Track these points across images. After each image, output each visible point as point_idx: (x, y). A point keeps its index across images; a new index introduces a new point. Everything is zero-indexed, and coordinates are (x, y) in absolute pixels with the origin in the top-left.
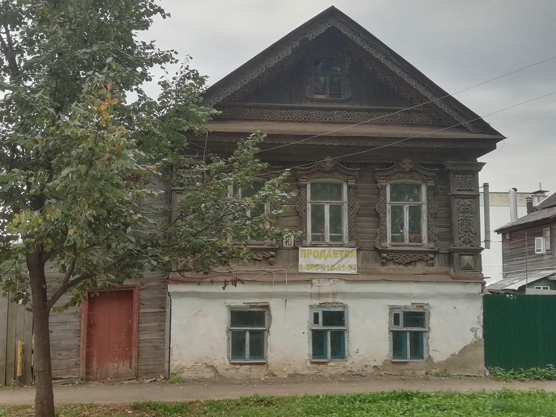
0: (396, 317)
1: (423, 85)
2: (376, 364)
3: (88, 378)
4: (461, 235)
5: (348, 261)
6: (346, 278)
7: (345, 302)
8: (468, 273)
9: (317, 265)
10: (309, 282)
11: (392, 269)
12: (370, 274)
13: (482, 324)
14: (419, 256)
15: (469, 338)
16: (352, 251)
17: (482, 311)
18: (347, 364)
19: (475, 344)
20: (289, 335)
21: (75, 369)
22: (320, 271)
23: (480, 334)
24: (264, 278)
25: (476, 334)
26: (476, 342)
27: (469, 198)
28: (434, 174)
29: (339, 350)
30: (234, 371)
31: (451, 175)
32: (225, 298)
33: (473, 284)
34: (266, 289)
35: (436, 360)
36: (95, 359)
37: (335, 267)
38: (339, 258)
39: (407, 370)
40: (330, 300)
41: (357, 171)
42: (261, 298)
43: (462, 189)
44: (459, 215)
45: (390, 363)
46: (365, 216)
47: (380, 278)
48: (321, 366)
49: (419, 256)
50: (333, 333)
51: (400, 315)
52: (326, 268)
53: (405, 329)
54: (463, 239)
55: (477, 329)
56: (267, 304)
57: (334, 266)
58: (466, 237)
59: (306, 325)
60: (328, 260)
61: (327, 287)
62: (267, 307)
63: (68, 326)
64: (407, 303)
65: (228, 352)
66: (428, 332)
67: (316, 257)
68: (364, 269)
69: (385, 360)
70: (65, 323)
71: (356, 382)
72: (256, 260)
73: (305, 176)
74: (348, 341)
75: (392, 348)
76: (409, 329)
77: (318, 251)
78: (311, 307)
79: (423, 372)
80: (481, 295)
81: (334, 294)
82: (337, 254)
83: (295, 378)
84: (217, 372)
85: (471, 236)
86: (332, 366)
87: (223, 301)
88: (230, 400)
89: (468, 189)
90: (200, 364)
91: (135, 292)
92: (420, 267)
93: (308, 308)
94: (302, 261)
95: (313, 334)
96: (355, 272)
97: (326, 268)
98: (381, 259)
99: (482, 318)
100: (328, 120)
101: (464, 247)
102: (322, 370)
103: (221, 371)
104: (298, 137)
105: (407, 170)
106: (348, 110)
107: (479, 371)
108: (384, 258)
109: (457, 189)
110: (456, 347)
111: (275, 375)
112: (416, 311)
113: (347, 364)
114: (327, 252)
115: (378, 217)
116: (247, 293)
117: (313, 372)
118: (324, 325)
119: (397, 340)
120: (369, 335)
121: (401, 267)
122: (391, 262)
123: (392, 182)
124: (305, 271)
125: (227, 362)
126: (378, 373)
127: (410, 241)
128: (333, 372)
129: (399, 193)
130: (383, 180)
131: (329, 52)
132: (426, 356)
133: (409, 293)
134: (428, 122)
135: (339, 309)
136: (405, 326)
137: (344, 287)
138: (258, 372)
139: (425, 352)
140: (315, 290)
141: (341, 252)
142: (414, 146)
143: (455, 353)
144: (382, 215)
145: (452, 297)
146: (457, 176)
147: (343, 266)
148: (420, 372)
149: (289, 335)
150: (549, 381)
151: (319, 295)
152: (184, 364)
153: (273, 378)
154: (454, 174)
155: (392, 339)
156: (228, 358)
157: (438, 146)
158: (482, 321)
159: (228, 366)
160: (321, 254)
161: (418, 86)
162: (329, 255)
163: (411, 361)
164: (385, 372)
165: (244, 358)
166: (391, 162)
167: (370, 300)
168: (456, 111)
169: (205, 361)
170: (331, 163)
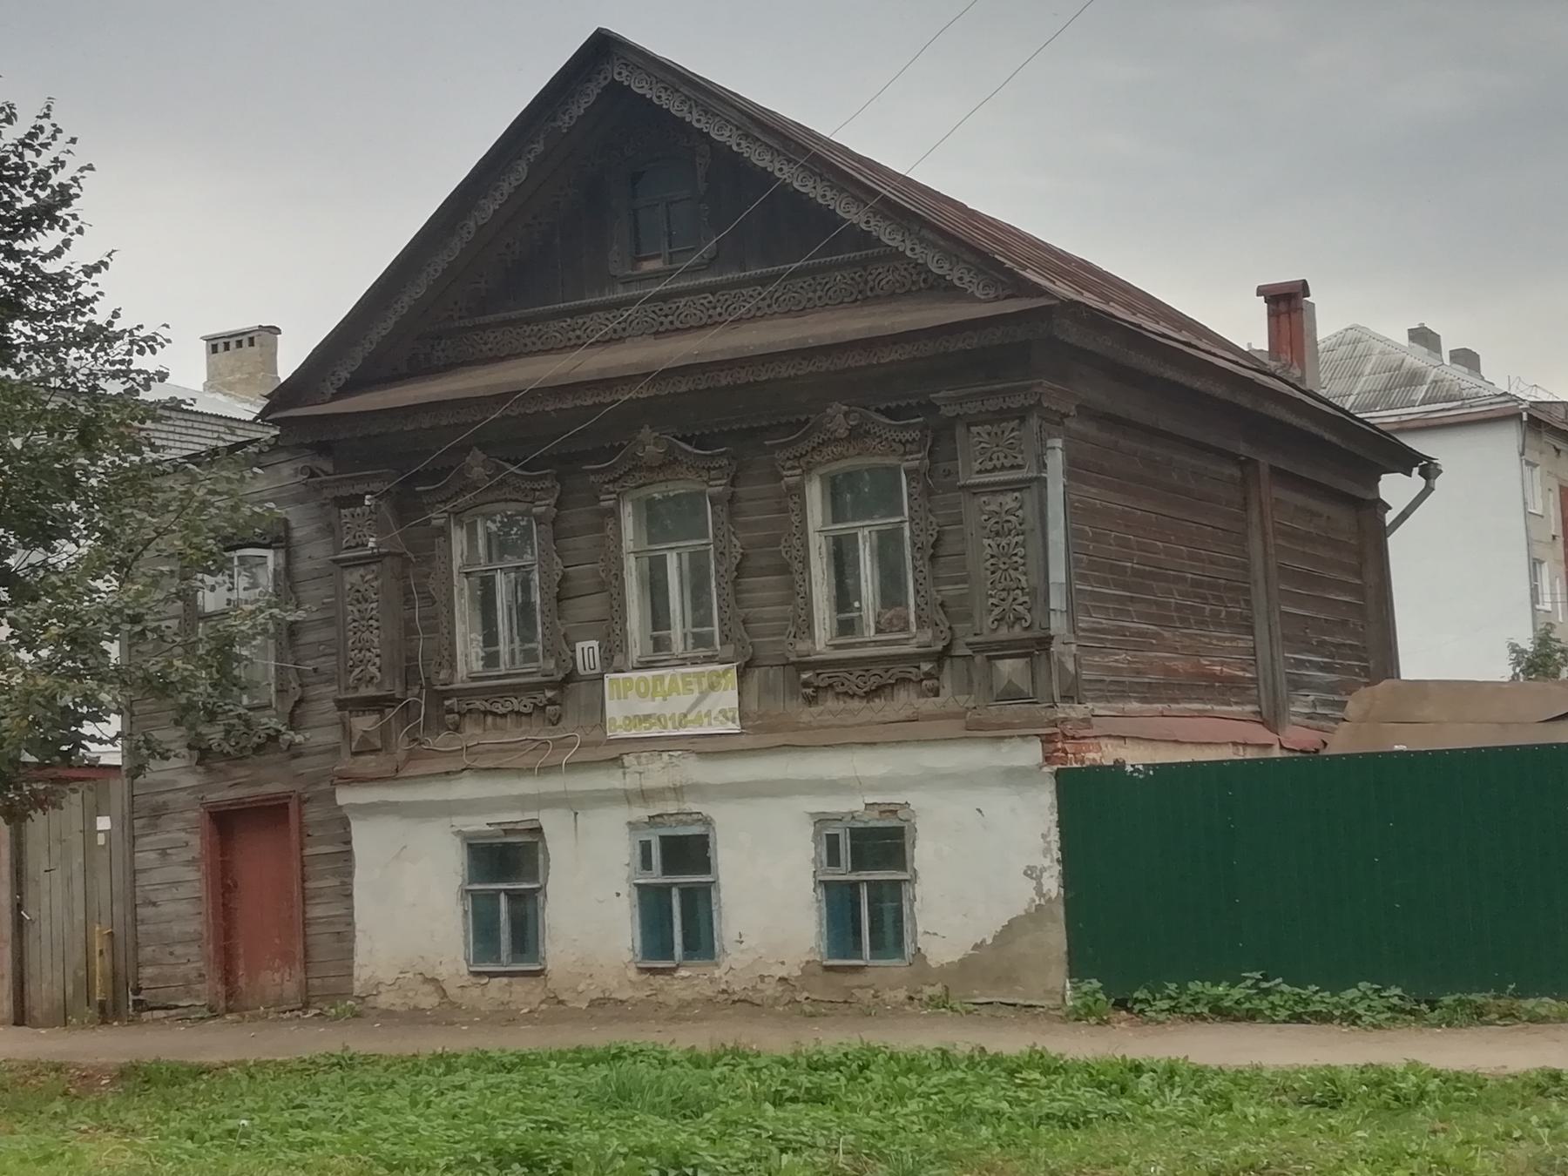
0: (833, 841)
1: (842, 190)
2: (784, 974)
3: (231, 1001)
4: (991, 600)
5: (707, 699)
6: (697, 748)
7: (706, 809)
8: (1012, 710)
9: (647, 717)
10: (617, 761)
11: (831, 712)
12: (771, 729)
13: (1057, 854)
14: (897, 670)
15: (1021, 897)
16: (726, 671)
17: (1055, 817)
18: (717, 973)
19: (1036, 915)
20: (590, 902)
21: (198, 987)
22: (655, 732)
23: (1052, 885)
24: (528, 760)
27: (1014, 490)
28: (916, 435)
29: (701, 943)
30: (476, 992)
31: (960, 431)
34: (553, 784)
35: (933, 962)
36: (241, 963)
37: (690, 717)
38: (696, 694)
39: (860, 987)
40: (671, 808)
41: (722, 454)
42: (523, 809)
43: (989, 465)
44: (986, 542)
45: (819, 970)
46: (762, 572)
47: (779, 739)
48: (660, 980)
49: (897, 670)
50: (688, 893)
52: (670, 724)
53: (853, 877)
54: (997, 611)
55: (1043, 870)
56: (535, 825)
57: (685, 716)
58: (1005, 605)
59: (624, 873)
60: (670, 699)
61: (657, 773)
63: (183, 892)
64: (850, 804)
65: (467, 945)
66: (912, 881)
67: (643, 696)
68: (760, 717)
70: (176, 884)
71: (1535, 1019)
72: (518, 713)
73: (610, 487)
74: (720, 914)
75: (824, 930)
76: (864, 876)
78: (633, 826)
79: (902, 995)
80: (1046, 769)
81: (678, 791)
82: (690, 683)
83: (604, 1007)
84: (445, 995)
85: (1021, 600)
86: (683, 978)
87: (446, 821)
88: (1138, 1069)
89: (1007, 463)
90: (410, 975)
91: (293, 807)
92: (905, 701)
95: (641, 897)
96: (734, 727)
97: (670, 724)
98: (801, 691)
100: (667, 326)
101: (1004, 633)
102: (661, 990)
103: (452, 991)
104: (502, 398)
105: (842, 433)
106: (713, 289)
107: (1046, 992)
108: (806, 684)
109: (976, 466)
110: (986, 926)
111: (561, 1002)
112: (880, 824)
113: (717, 973)
114: (667, 681)
115: (791, 571)
116: (774, 783)
117: (642, 994)
118: (665, 872)
119: (840, 904)
120: (769, 897)
121: (855, 704)
122: (830, 694)
123: (823, 471)
125: (464, 970)
126: (793, 1000)
127: (879, 631)
128: (688, 995)
129: (657, 522)
130: (793, 468)
131: (616, 155)
132: (909, 949)
133: (863, 774)
134: (914, 283)
136: (858, 865)
137: (696, 771)
138: (523, 994)
139: (907, 939)
140: (631, 782)
141: (699, 675)
142: (832, 368)
143: (984, 941)
144: (797, 566)
145: (968, 780)
146: (973, 429)
147: (708, 714)
148: (892, 994)
149: (590, 902)
150: (1325, 1026)
151: (645, 796)
152: (380, 975)
153: (556, 1009)
154: (969, 425)
155: (824, 904)
156: (467, 960)
157: (895, 357)
158: (1055, 846)
159: (467, 980)
160: (655, 687)
161: (829, 194)
162: (673, 689)
163: (872, 963)
164: (806, 994)
165: (498, 960)
166: (803, 418)
167: (765, 801)
168: (935, 245)
169: (420, 969)
170: (656, 444)
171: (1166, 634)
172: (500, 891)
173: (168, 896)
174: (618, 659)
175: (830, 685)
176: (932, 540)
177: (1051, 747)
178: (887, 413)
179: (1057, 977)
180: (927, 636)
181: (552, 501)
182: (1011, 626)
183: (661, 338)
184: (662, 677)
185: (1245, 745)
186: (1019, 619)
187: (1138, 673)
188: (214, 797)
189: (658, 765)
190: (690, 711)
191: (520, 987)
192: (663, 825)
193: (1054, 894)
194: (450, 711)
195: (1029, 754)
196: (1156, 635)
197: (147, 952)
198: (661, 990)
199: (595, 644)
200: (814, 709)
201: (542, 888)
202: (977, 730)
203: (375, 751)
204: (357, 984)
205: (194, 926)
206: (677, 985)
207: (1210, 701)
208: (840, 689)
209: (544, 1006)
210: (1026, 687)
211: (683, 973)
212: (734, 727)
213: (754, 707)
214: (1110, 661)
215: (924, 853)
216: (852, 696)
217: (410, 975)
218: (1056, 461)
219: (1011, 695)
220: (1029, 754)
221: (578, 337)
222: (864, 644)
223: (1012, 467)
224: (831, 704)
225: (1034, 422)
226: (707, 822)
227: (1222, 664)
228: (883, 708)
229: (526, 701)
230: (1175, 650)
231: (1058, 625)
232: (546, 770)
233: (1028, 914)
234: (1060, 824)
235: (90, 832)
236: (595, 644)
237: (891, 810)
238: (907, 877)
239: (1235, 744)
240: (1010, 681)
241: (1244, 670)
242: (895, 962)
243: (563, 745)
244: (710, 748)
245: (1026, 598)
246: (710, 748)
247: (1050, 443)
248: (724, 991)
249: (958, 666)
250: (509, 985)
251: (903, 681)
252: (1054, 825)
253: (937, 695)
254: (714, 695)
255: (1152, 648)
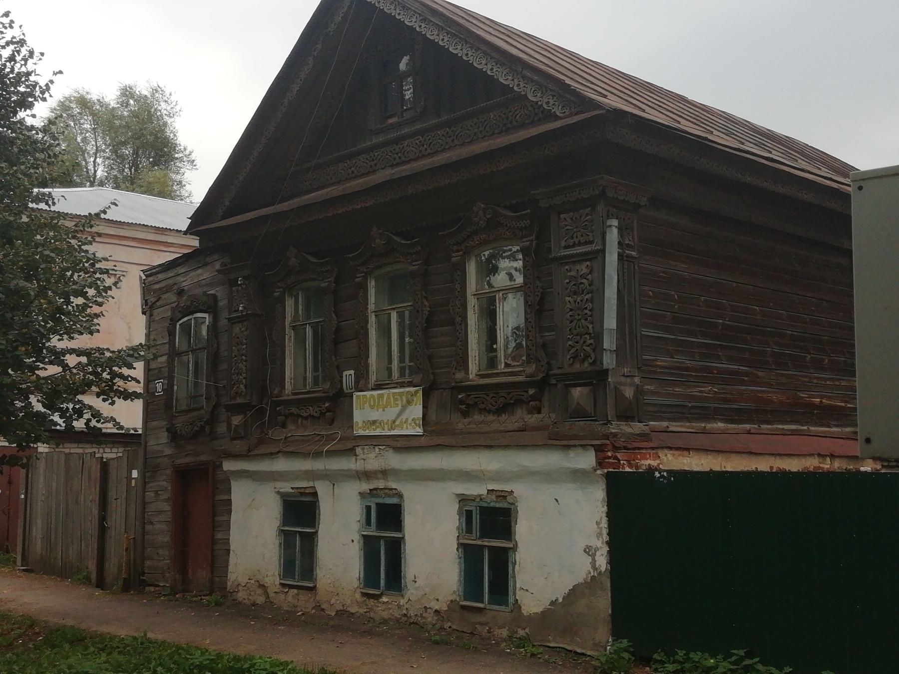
1: (478, 49)
2: (437, 607)
4: (570, 343)
9: (374, 422)
10: (351, 451)
13: (605, 537)
16: (416, 392)
17: (605, 509)
18: (402, 602)
19: (590, 585)
22: (378, 432)
23: (602, 562)
25: (594, 561)
26: (593, 577)
27: (586, 260)
29: (395, 580)
30: (282, 597)
32: (275, 480)
33: (580, 450)
34: (317, 465)
37: (397, 423)
38: (400, 407)
40: (381, 484)
43: (571, 242)
44: (568, 299)
48: (372, 602)
51: (474, 513)
53: (479, 542)
54: (573, 350)
55: (597, 549)
57: (394, 422)
59: (356, 527)
61: (372, 460)
62: (315, 494)
63: (162, 517)
69: (452, 601)
76: (487, 542)
77: (372, 396)
78: (362, 495)
79: (505, 633)
80: (599, 472)
81: (384, 473)
84: (268, 597)
85: (589, 342)
86: (384, 603)
87: (272, 484)
90: (253, 581)
92: (521, 417)
93: (359, 498)
94: (358, 416)
96: (419, 431)
98: (462, 408)
99: (604, 524)
101: (577, 367)
103: (272, 595)
105: (483, 224)
106: (421, 133)
107: (594, 644)
108: (461, 402)
109: (563, 243)
111: (323, 610)
117: (362, 611)
121: (491, 417)
124: (362, 432)
128: (385, 615)
130: (458, 251)
132: (511, 600)
133: (486, 468)
135: (394, 501)
136: (484, 535)
137: (394, 461)
138: (305, 603)
139: (511, 593)
141: (401, 394)
143: (557, 600)
144: (458, 319)
145: (548, 476)
146: (562, 216)
151: (365, 475)
154: (560, 213)
156: (280, 575)
158: (605, 532)
164: (449, 624)
171: (760, 374)
172: (296, 532)
173: (157, 519)
174: (362, 382)
175: (476, 403)
176: (538, 298)
177: (601, 455)
178: (511, 208)
179: (603, 634)
180: (531, 369)
181: (332, 279)
182: (583, 361)
183: (410, 174)
184: (382, 396)
185: (832, 456)
186: (587, 356)
187: (726, 401)
188: (178, 461)
189: (373, 455)
190: (397, 418)
191: (303, 596)
192: (378, 496)
193: (603, 569)
194: (280, 414)
195: (586, 460)
196: (746, 374)
197: (149, 551)
198: (371, 609)
199: (352, 372)
200: (466, 420)
201: (317, 532)
202: (560, 440)
203: (241, 438)
204: (229, 584)
205: (167, 539)
206: (381, 607)
207: (807, 423)
208: (482, 406)
209: (314, 611)
210: (589, 408)
211: (384, 599)
212: (419, 431)
213: (434, 418)
214: (695, 392)
215: (522, 529)
216: (489, 412)
217: (253, 581)
218: (613, 236)
219: (579, 414)
220: (586, 460)
221: (353, 172)
222: (498, 375)
223: (586, 243)
224: (477, 417)
225: (601, 208)
226: (400, 496)
227: (822, 397)
228: (511, 421)
229: (317, 409)
230: (770, 385)
231: (609, 361)
232: (317, 455)
233: (586, 582)
234: (609, 515)
235: (129, 478)
236: (352, 372)
237: (503, 496)
238: (511, 546)
239: (819, 455)
240: (578, 404)
241: (846, 402)
242: (503, 608)
243: (330, 438)
244: (404, 445)
245: (592, 341)
246: (404, 445)
247: (609, 222)
248: (405, 615)
249: (544, 395)
250: (297, 594)
251: (519, 402)
252: (604, 515)
253: (539, 412)
254: (410, 408)
255: (743, 383)
